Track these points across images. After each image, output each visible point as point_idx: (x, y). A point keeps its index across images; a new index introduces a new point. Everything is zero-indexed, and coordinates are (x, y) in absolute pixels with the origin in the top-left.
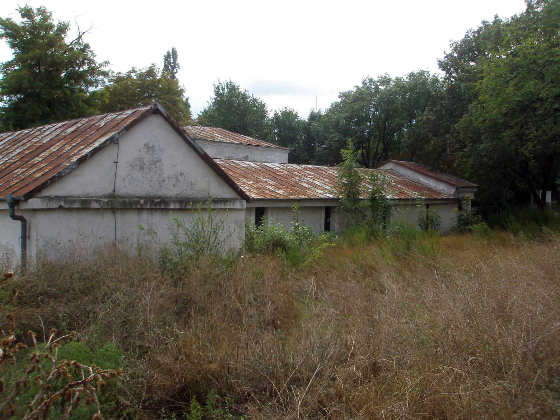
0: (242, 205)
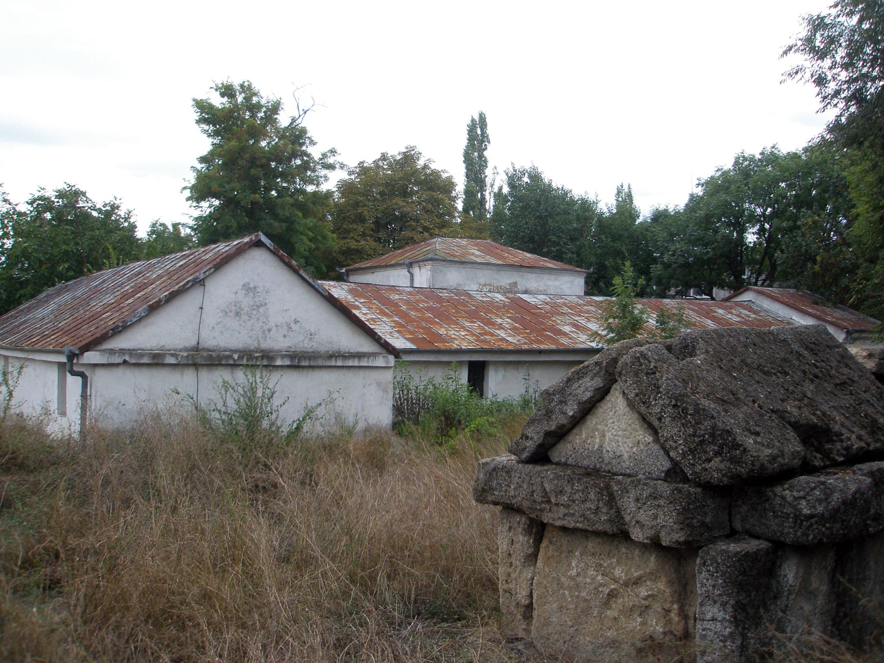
0: (387, 362)
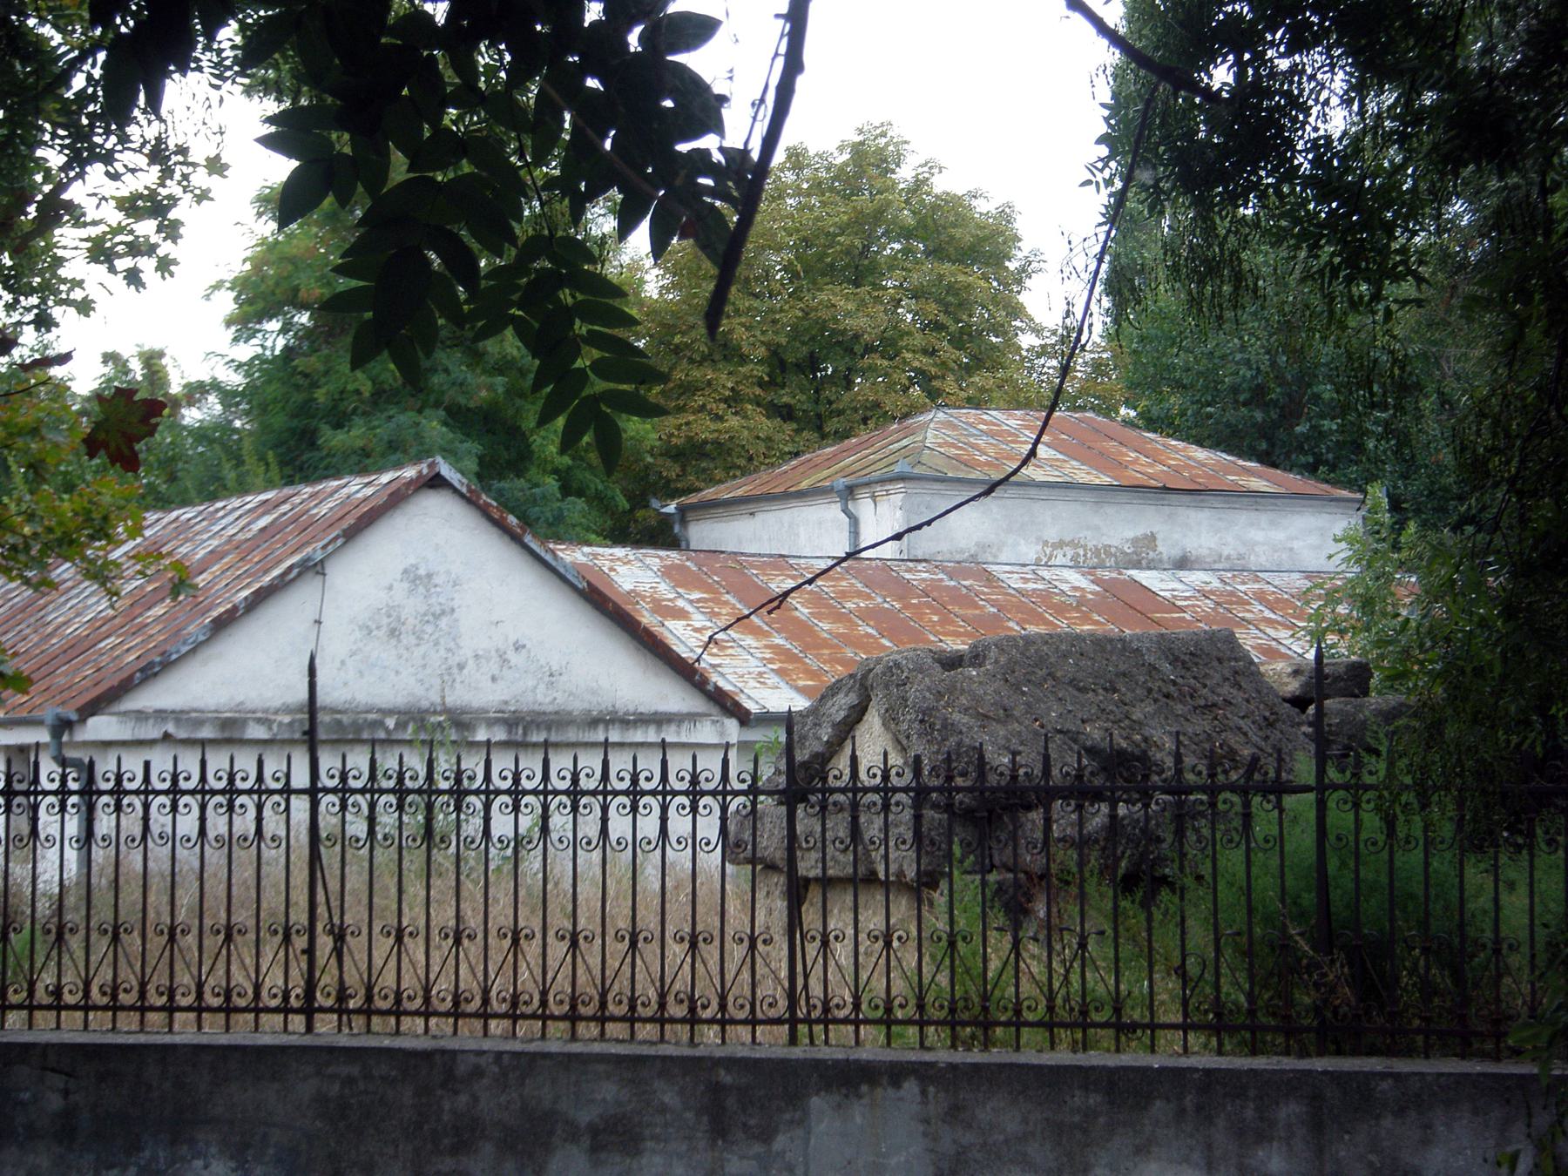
0: (722, 734)
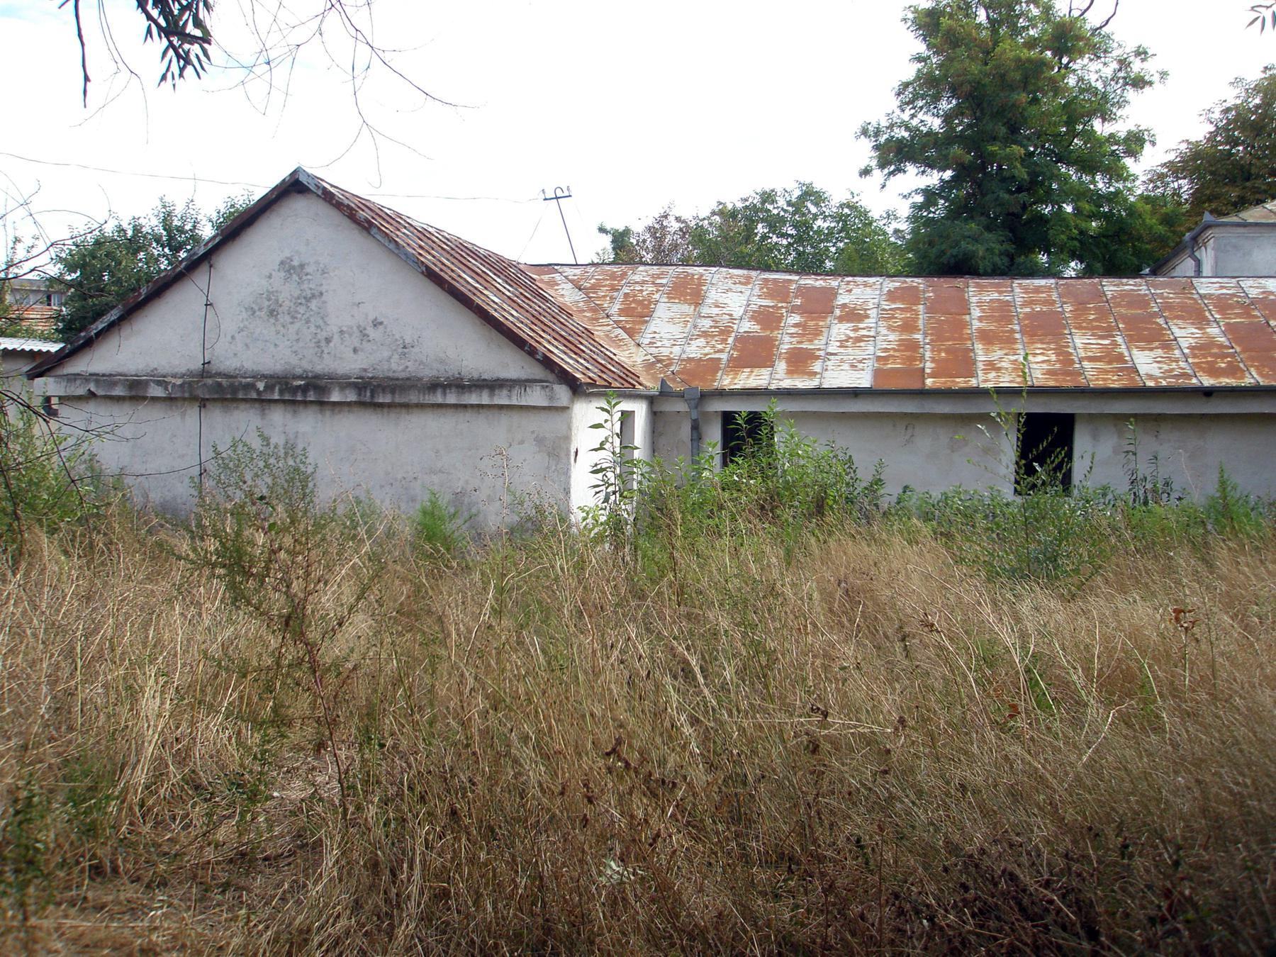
0: (551, 398)
